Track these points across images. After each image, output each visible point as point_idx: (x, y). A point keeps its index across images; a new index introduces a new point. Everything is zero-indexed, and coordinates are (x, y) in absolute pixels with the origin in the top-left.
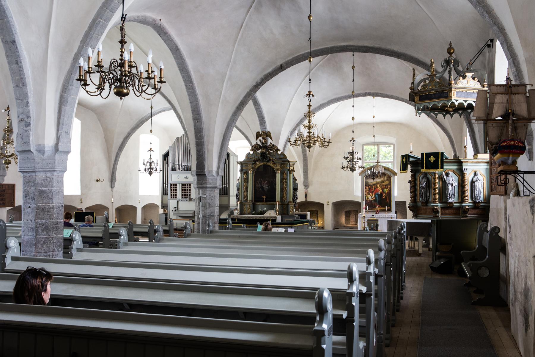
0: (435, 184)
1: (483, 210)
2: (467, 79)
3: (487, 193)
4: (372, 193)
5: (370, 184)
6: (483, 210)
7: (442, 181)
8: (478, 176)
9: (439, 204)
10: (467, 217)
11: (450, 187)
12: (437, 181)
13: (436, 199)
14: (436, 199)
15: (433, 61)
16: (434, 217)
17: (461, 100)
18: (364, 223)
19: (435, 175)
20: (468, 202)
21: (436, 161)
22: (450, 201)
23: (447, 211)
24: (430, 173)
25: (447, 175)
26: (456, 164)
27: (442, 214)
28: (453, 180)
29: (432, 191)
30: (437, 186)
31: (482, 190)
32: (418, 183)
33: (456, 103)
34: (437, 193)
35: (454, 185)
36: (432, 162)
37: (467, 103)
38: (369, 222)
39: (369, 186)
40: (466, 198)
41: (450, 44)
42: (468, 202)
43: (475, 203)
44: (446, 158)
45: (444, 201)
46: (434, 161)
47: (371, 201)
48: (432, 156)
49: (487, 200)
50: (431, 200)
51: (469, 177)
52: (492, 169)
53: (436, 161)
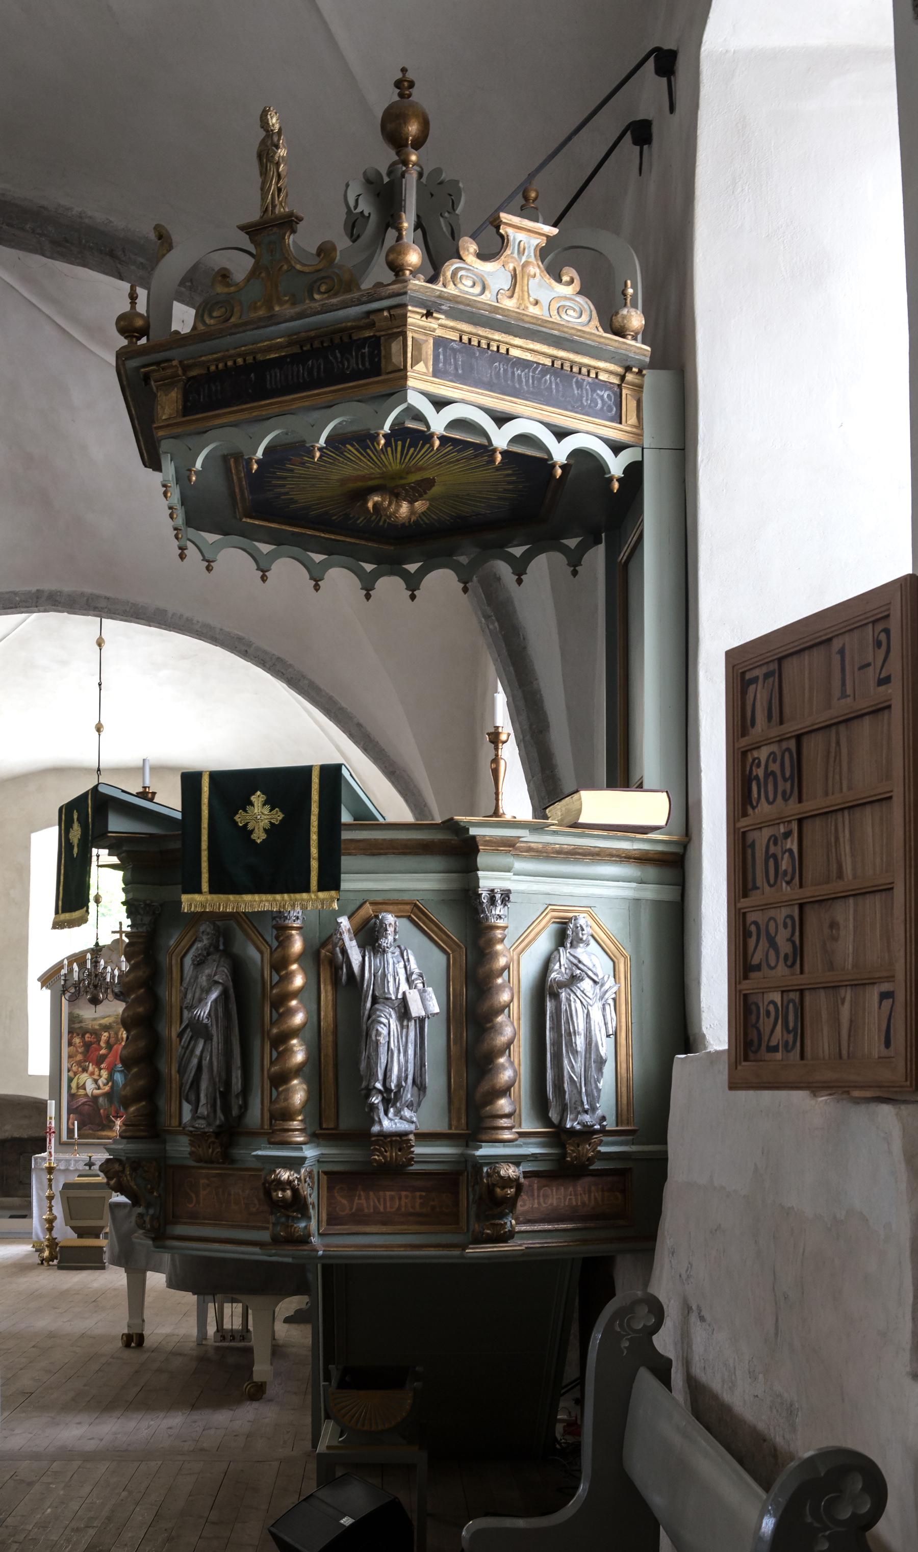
0: (280, 1002)
1: (621, 1183)
2: (510, 259)
3: (636, 1066)
4: (98, 1064)
5: (89, 1025)
6: (621, 1183)
7: (335, 981)
8: (580, 952)
9: (310, 1153)
10: (511, 1235)
11: (388, 1025)
12: (298, 981)
13: (287, 1115)
14: (287, 1115)
15: (273, 121)
16: (276, 1241)
17: (469, 403)
18: (50, 1198)
19: (283, 940)
20: (514, 1141)
21: (289, 833)
22: (389, 1123)
23: (366, 1201)
24: (252, 919)
25: (370, 936)
26: (434, 862)
27: (333, 1219)
28: (410, 976)
29: (262, 1053)
30: (299, 1019)
31: (605, 1048)
32: (171, 995)
33: (438, 423)
34: (298, 1071)
35: (416, 1009)
36: (259, 836)
37: (513, 429)
38: (73, 1193)
39: (83, 1033)
40: (504, 1105)
41: (404, 85)
42: (514, 1141)
43: (558, 1136)
44: (364, 817)
45: (346, 1123)
46: (272, 830)
47: (95, 1098)
48: (258, 798)
49: (650, 1111)
50: (256, 1114)
51: (520, 955)
52: (761, 838)
53: (289, 833)
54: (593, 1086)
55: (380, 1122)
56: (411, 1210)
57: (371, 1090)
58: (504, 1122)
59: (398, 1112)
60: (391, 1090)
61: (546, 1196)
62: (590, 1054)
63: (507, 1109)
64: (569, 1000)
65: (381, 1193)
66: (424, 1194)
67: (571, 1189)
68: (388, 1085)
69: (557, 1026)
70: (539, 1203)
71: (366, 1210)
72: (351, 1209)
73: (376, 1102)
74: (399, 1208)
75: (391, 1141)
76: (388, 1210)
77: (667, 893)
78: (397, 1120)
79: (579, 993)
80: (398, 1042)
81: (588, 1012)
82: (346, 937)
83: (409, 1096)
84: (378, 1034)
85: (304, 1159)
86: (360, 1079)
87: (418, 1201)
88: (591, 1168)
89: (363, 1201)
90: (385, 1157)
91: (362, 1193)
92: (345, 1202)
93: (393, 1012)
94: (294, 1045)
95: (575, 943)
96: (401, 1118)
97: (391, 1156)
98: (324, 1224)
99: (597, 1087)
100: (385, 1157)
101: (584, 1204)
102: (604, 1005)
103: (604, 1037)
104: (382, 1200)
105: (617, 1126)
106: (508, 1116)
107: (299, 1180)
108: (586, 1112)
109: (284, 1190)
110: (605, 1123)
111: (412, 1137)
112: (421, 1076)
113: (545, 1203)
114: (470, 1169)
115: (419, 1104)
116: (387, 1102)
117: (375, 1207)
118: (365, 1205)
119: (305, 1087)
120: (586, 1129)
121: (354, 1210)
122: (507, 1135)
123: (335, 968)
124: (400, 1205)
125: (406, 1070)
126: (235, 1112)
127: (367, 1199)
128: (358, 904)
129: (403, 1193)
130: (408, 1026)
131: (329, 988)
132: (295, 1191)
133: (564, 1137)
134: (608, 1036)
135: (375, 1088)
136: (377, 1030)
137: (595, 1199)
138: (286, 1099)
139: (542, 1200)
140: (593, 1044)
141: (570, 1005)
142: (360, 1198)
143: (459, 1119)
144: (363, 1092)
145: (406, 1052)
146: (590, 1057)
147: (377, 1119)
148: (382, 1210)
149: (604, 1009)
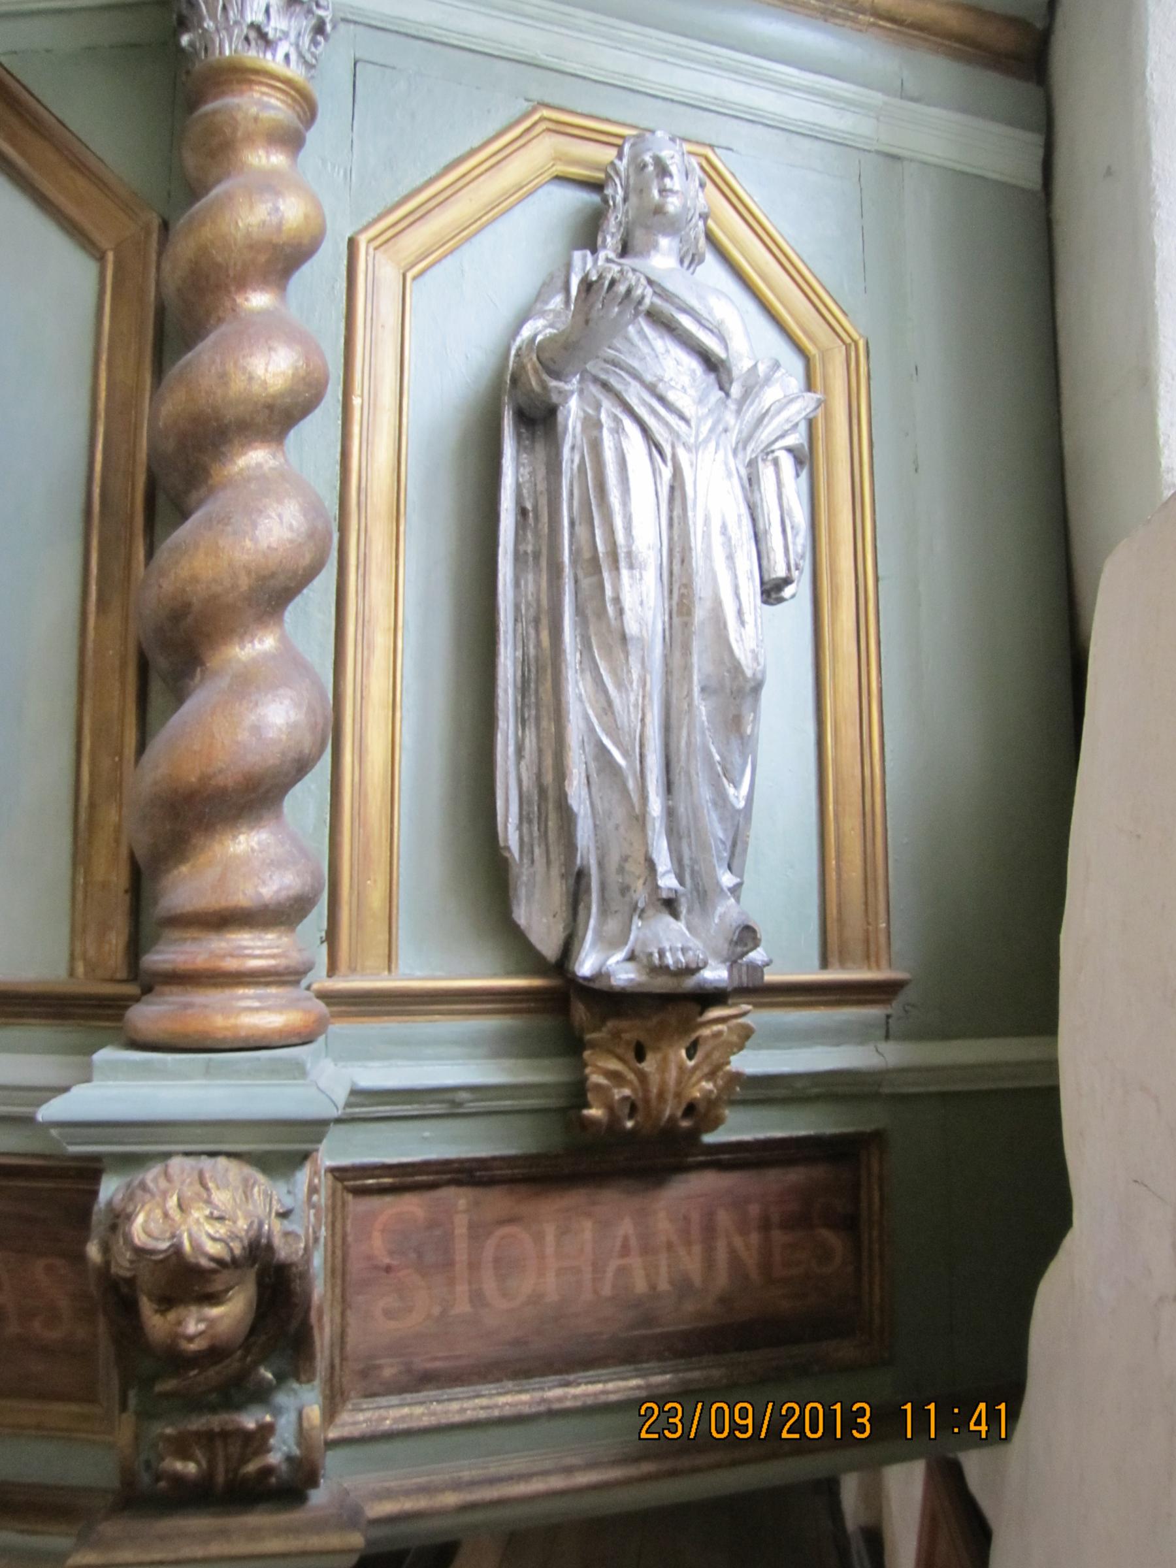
31: (768, 643)
43: (562, 1009)
54: (705, 794)
58: (257, 948)
61: (505, 1266)
62: (687, 650)
63: (273, 886)
64: (592, 425)
67: (626, 1227)
69: (541, 557)
70: (477, 1297)
77: (1002, 153)
79: (634, 394)
81: (677, 472)
88: (709, 1138)
95: (639, 235)
99: (721, 799)
101: (684, 1288)
102: (752, 464)
103: (751, 591)
105: (825, 964)
106: (282, 915)
108: (670, 905)
110: (757, 956)
113: (505, 1294)
120: (662, 984)
122: (258, 1012)
133: (580, 1012)
134: (772, 591)
137: (732, 1251)
139: (489, 1285)
140: (700, 613)
141: (596, 446)
146: (687, 668)
149: (752, 481)
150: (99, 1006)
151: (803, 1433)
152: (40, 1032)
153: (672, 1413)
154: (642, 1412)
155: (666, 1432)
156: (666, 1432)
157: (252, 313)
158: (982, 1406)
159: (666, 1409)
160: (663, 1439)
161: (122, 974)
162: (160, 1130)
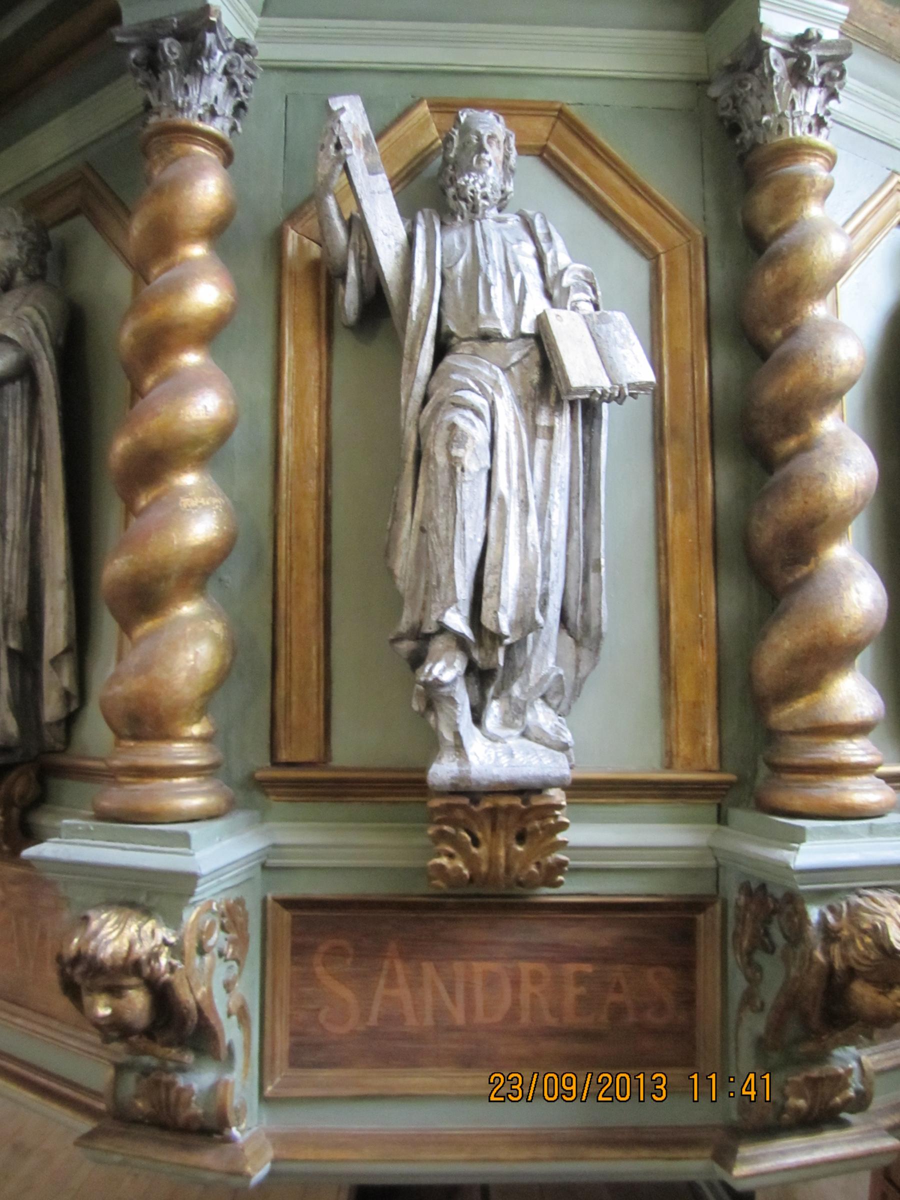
22: (490, 751)
25: (433, 189)
34: (200, 573)
35: (581, 369)
45: (355, 746)
55: (459, 747)
56: (551, 1021)
57: (428, 638)
58: (854, 750)
59: (516, 713)
60: (497, 637)
65: (458, 967)
66: (588, 968)
68: (486, 619)
71: (411, 1021)
72: (364, 1016)
73: (447, 677)
74: (513, 1015)
75: (493, 812)
76: (480, 1018)
78: (514, 740)
80: (522, 476)
82: (357, 160)
83: (551, 661)
84: (454, 434)
85: (182, 885)
86: (397, 602)
87: (572, 992)
89: (403, 992)
90: (471, 861)
91: (399, 966)
92: (345, 993)
93: (502, 378)
94: (184, 491)
96: (524, 735)
97: (492, 861)
98: (281, 1061)
100: (471, 861)
104: (460, 996)
107: (176, 950)
109: (115, 991)
111: (557, 796)
112: (585, 600)
114: (734, 896)
115: (578, 688)
116: (799, 75)
117: (440, 1011)
118: (408, 1007)
119: (217, 628)
121: (373, 1021)
123: (326, 277)
124: (516, 1003)
125: (371, 846)
126: (52, 708)
127: (415, 984)
128: (398, 108)
129: (526, 967)
130: (551, 430)
131: (309, 337)
132: (162, 995)
135: (443, 629)
136: (453, 426)
138: (144, 668)
142: (392, 981)
143: (696, 735)
144: (406, 646)
145: (543, 515)
147: (448, 736)
148: (460, 1018)
150: (702, 789)
151: (614, 1096)
152: (651, 807)
153: (515, 1080)
154: (600, 1081)
155: (510, 1096)
156: (510, 1096)
157: (186, 369)
158: (752, 1076)
159: (510, 1078)
160: (507, 1100)
161: (716, 767)
162: (833, 874)
